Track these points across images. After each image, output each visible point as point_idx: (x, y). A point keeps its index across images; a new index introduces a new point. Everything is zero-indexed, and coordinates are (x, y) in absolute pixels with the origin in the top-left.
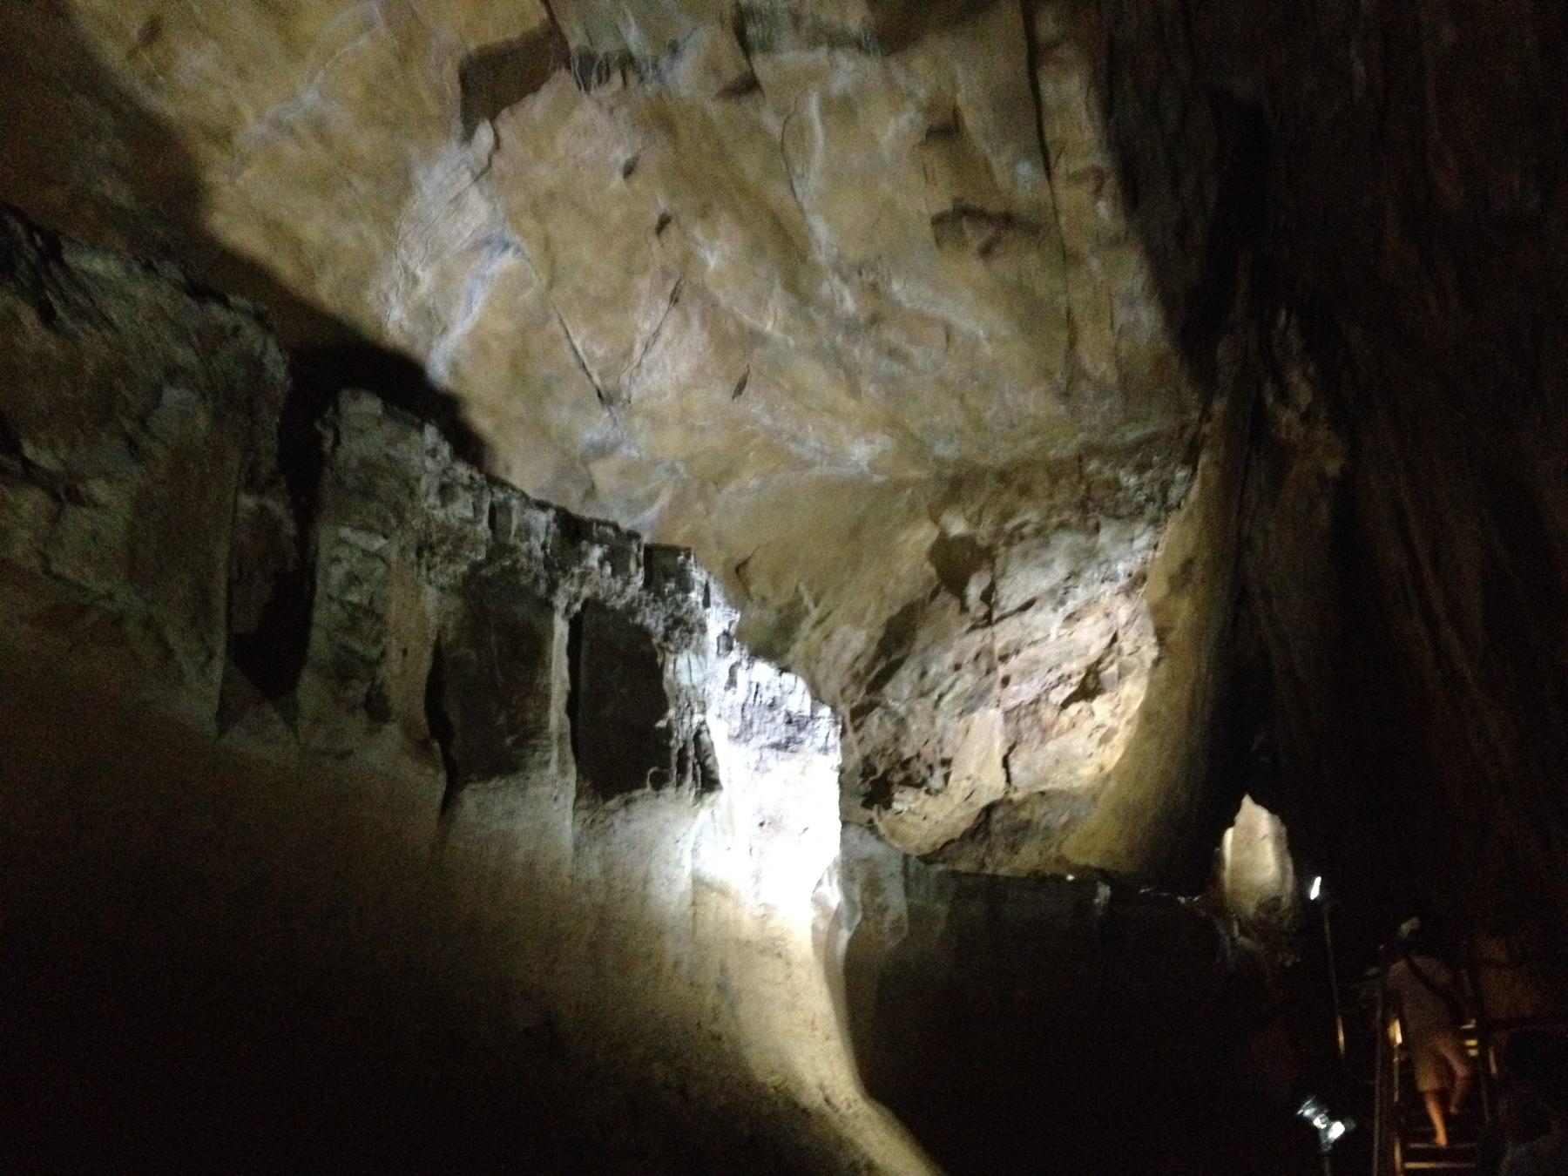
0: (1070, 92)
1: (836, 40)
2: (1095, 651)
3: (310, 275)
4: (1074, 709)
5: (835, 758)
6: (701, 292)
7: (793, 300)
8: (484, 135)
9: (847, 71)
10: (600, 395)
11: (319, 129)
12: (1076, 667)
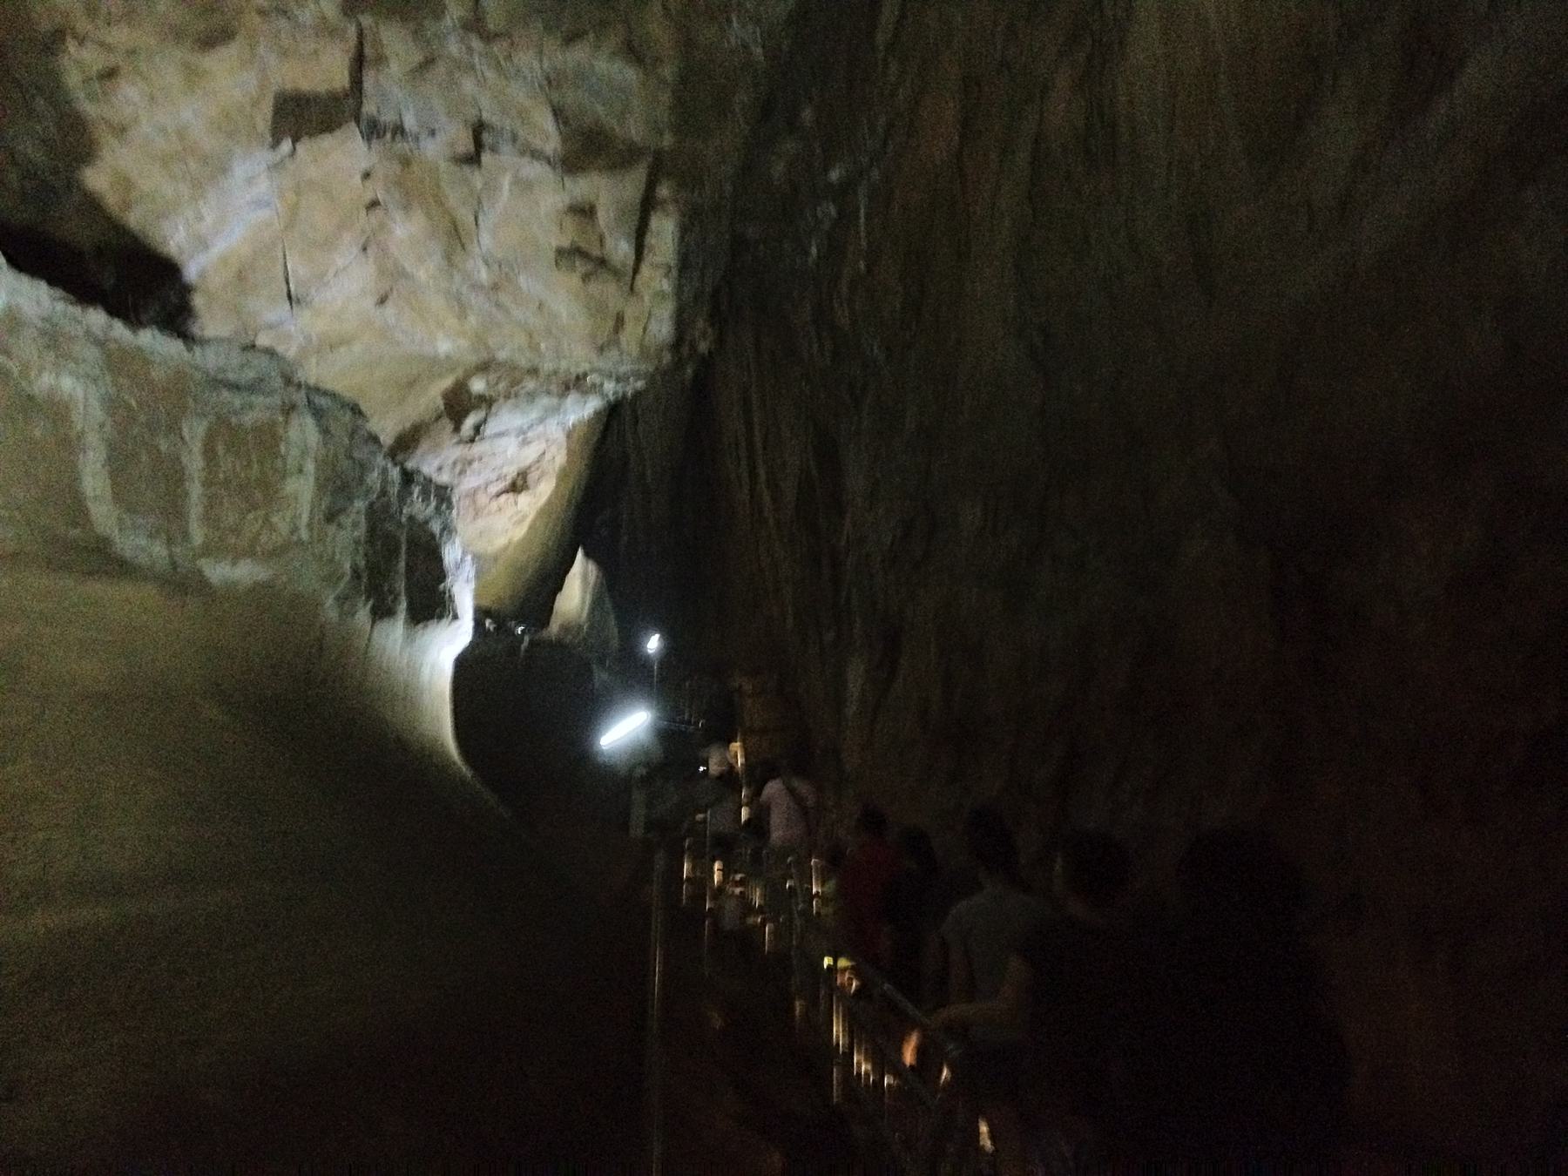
0: (665, 230)
1: (536, 154)
2: (527, 463)
3: (127, 205)
4: (503, 498)
5: (472, 585)
6: (384, 252)
7: (444, 263)
8: (286, 146)
9: (534, 170)
10: (290, 297)
11: (181, 134)
12: (511, 472)
